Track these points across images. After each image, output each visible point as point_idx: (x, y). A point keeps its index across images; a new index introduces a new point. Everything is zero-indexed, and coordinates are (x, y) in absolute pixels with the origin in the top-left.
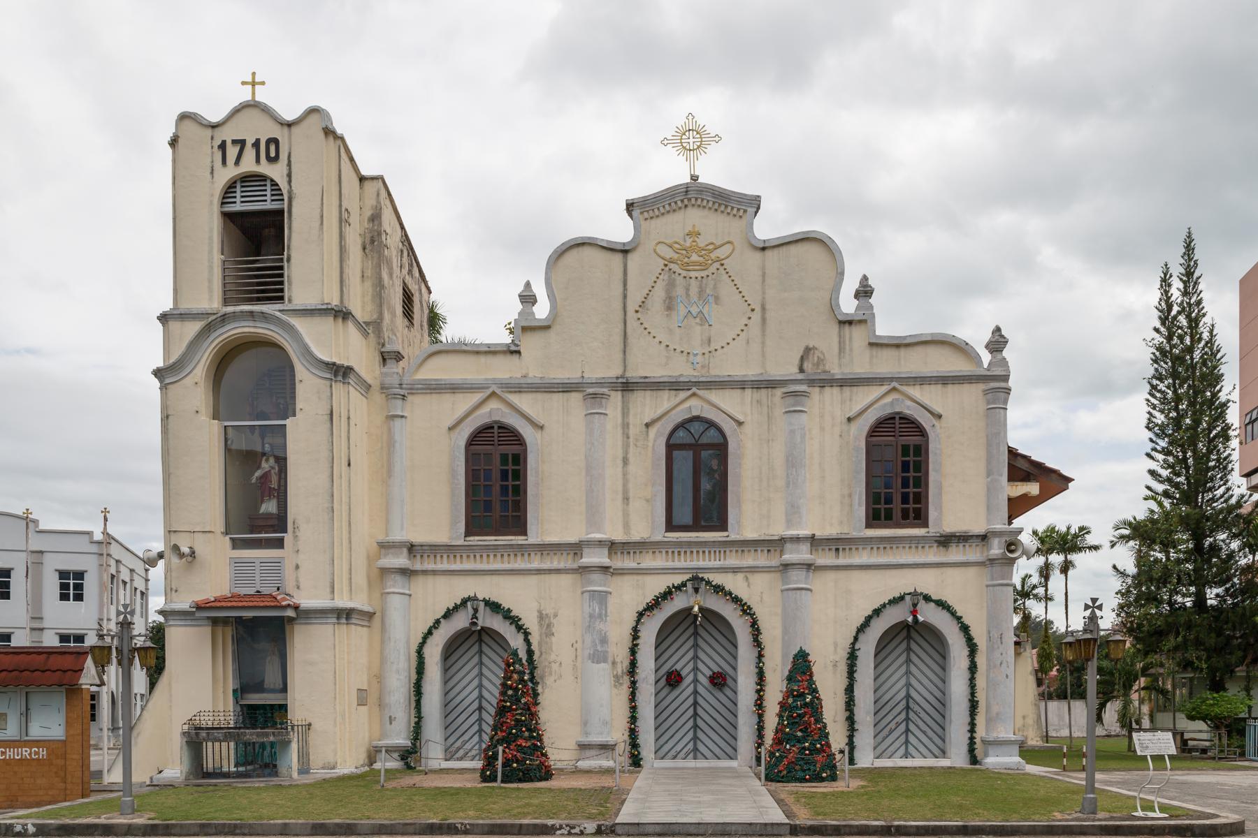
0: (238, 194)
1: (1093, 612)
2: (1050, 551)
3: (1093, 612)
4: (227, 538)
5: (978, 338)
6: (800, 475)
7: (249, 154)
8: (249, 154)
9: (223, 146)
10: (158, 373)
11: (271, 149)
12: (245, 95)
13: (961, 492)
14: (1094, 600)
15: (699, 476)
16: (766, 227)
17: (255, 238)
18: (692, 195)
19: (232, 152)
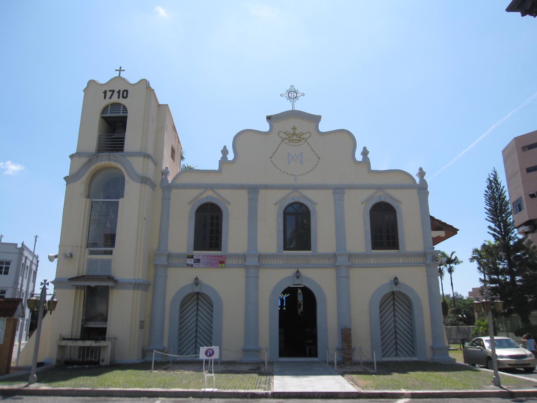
0: (109, 110)
7: (116, 94)
8: (116, 94)
12: (117, 74)
15: (298, 228)
19: (109, 94)
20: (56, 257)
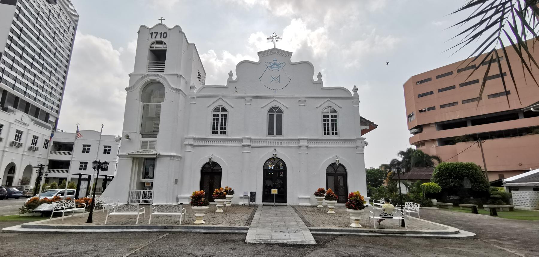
4: (21, 142)
5: (350, 89)
6: (303, 123)
7: (159, 35)
8: (159, 35)
9: (152, 34)
11: (165, 35)
12: (160, 22)
13: (347, 128)
15: (275, 123)
16: (293, 60)
17: (159, 56)
18: (275, 52)
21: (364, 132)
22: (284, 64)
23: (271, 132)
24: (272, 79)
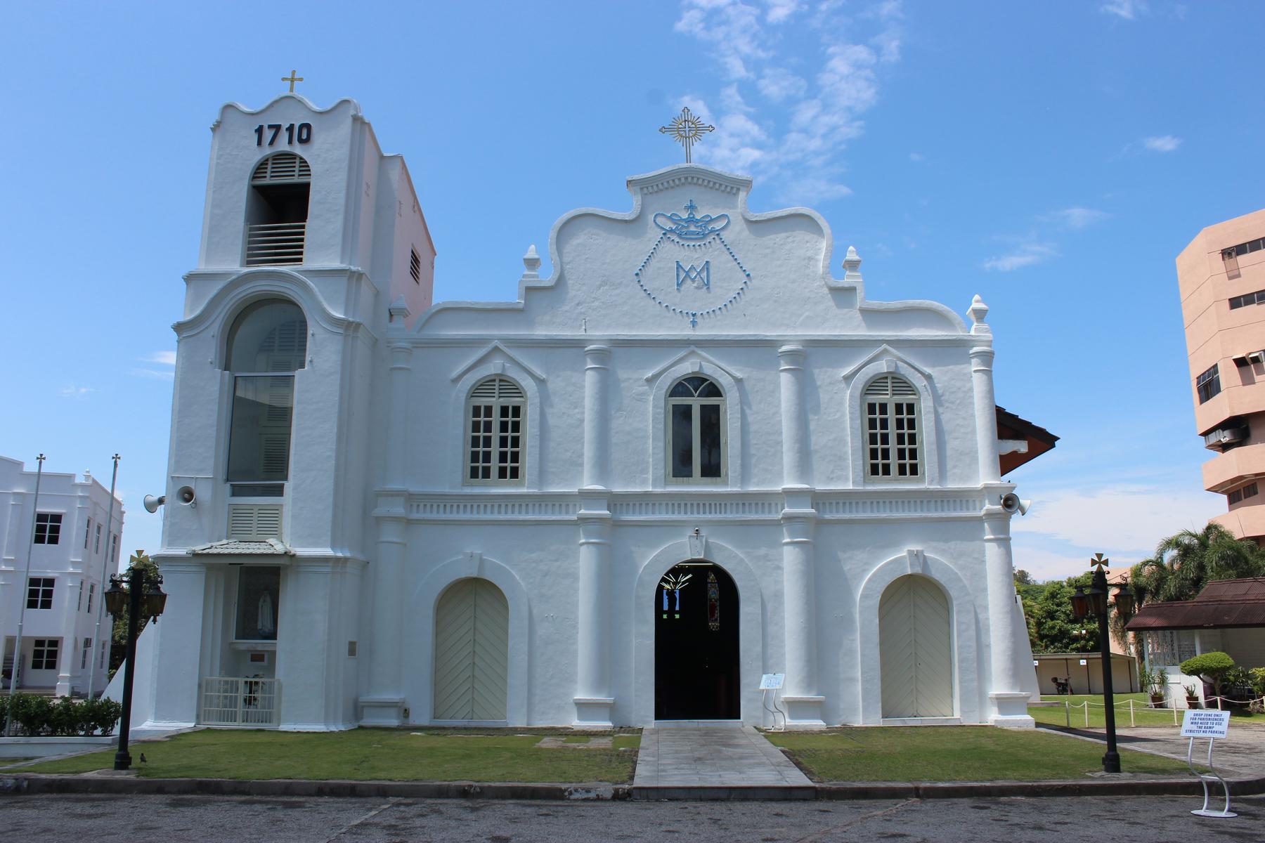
0: (269, 171)
1: (1100, 567)
2: (981, 693)
3: (1100, 567)
4: (228, 485)
7: (284, 136)
8: (284, 136)
10: (179, 328)
14: (1100, 556)
15: (698, 432)
17: (279, 205)
20: (161, 501)
21: (1008, 463)
22: (723, 223)
23: (681, 466)
24: (682, 275)
